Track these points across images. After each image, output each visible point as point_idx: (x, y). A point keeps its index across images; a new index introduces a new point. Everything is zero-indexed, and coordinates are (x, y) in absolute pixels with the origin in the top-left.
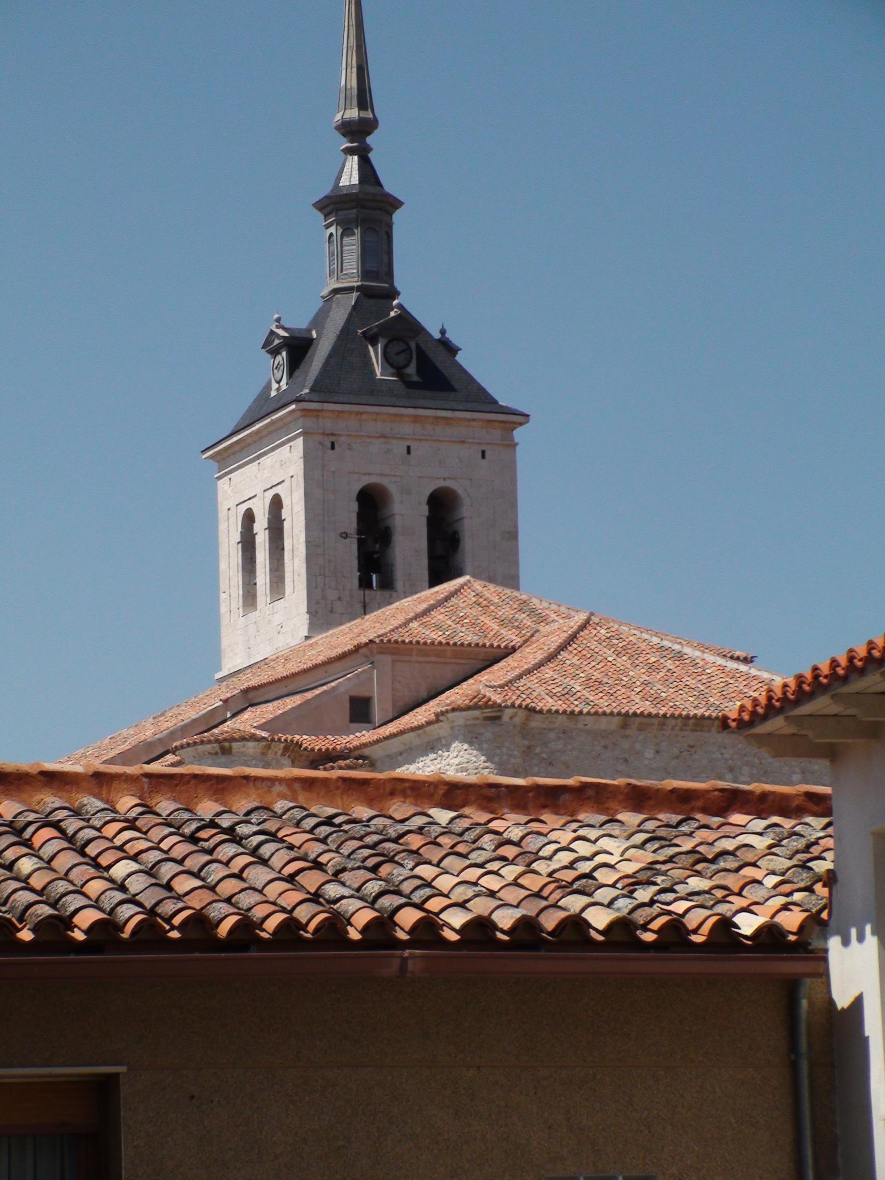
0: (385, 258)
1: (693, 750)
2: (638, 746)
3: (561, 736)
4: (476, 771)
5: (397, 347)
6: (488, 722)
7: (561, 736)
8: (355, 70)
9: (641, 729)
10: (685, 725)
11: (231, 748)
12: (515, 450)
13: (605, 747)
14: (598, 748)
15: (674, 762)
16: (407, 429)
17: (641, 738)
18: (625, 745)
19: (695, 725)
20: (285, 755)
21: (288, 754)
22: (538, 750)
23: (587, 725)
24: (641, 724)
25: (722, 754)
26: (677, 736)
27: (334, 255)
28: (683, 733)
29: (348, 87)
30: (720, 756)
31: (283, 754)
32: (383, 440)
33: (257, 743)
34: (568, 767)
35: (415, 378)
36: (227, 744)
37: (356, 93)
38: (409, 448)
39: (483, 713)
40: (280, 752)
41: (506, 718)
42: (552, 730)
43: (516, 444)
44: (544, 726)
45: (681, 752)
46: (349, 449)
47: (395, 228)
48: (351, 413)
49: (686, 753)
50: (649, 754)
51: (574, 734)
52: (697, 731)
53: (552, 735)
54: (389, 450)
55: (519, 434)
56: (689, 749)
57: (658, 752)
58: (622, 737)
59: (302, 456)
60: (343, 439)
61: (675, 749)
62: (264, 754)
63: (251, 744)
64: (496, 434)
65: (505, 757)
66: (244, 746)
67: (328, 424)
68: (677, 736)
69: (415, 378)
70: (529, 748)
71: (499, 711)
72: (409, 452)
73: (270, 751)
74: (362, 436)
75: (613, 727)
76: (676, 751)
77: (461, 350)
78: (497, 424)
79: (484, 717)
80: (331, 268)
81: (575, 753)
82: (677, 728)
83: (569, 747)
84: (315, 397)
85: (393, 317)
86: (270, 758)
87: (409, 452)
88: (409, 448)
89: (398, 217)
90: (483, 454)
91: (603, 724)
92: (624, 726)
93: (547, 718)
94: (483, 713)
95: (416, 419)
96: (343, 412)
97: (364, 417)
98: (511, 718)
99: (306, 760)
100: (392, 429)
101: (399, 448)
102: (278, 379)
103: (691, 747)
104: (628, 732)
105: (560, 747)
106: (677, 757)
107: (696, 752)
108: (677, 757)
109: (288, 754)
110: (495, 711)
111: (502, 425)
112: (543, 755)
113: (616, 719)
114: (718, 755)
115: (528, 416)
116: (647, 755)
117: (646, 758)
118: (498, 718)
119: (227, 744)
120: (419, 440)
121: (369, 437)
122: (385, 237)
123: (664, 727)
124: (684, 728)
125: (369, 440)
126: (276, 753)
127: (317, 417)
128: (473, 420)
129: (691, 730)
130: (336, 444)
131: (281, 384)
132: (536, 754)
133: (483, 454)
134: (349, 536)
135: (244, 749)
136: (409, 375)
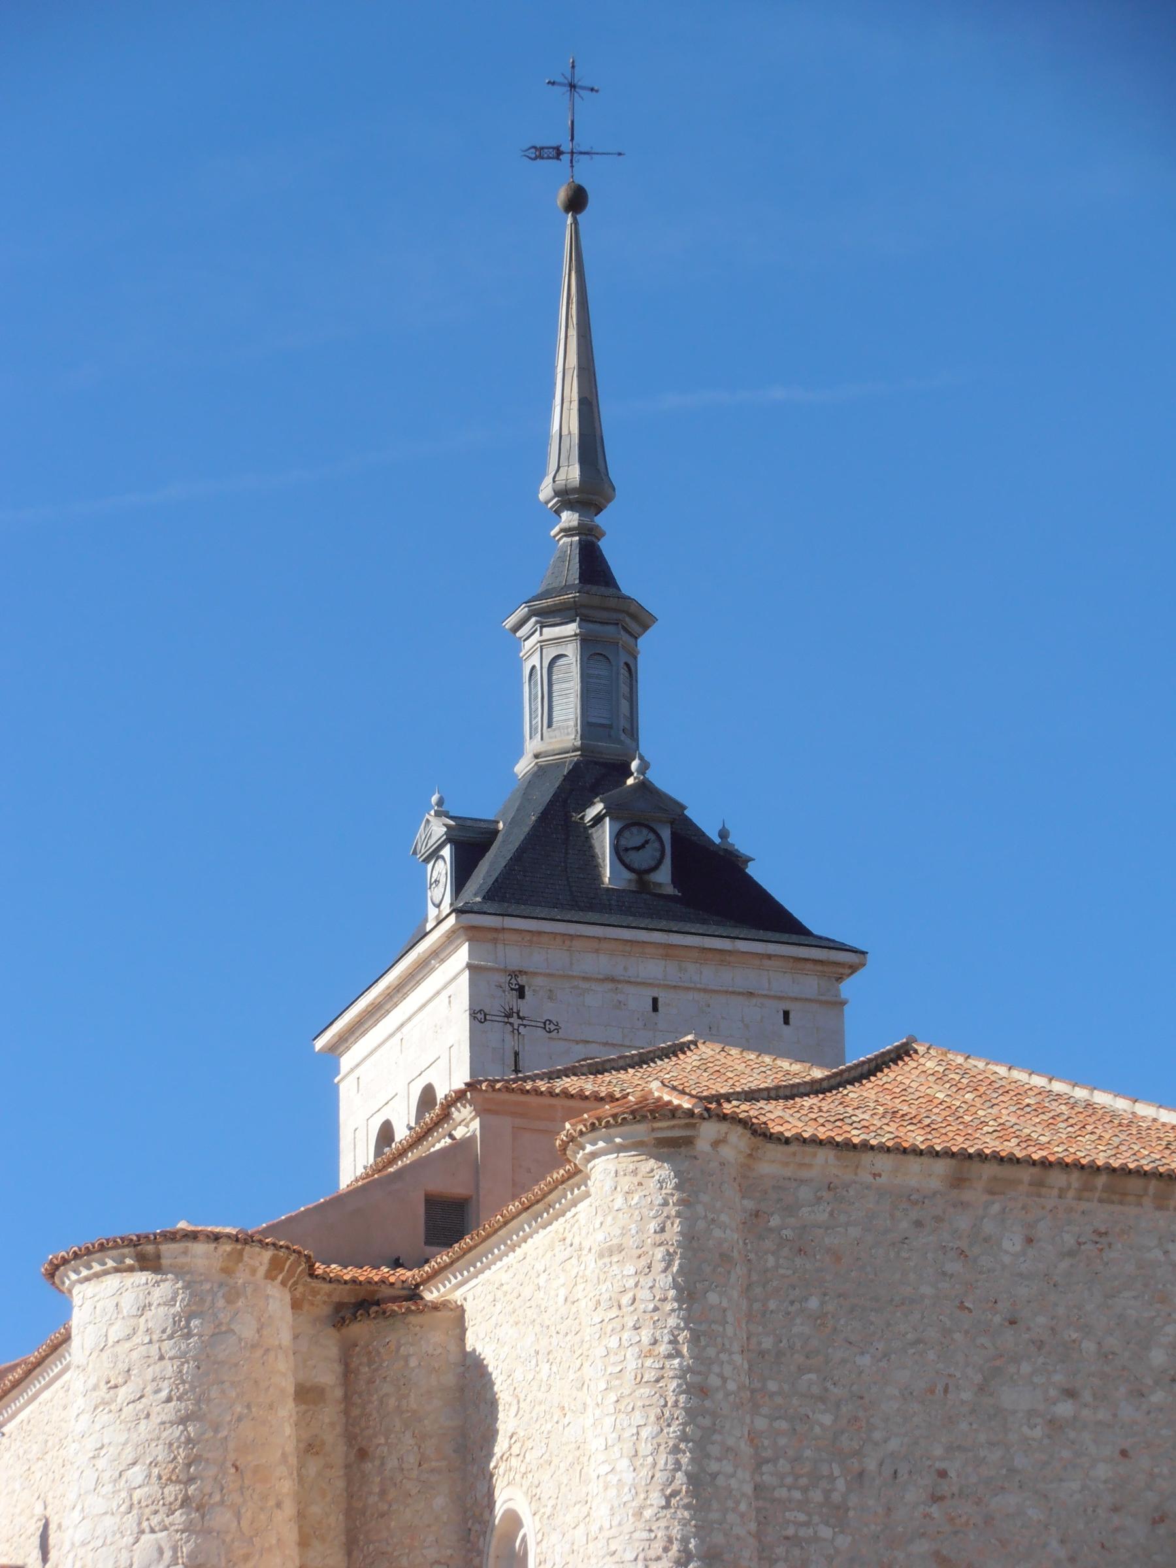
0: (624, 705)
1: (1103, 1240)
2: (988, 1227)
3: (824, 1194)
4: (640, 1251)
5: (635, 837)
6: (665, 1150)
7: (824, 1194)
8: (575, 405)
9: (994, 1189)
10: (1087, 1188)
11: (158, 1256)
12: (842, 1011)
13: (918, 1224)
14: (904, 1225)
15: (1064, 1265)
16: (652, 969)
17: (996, 1208)
18: (963, 1222)
19: (1107, 1188)
20: (273, 1279)
21: (280, 1278)
22: (775, 1221)
23: (880, 1175)
24: (995, 1179)
25: (1166, 1252)
26: (1070, 1210)
27: (537, 716)
28: (1084, 1205)
29: (565, 432)
30: (1162, 1259)
31: (270, 1276)
32: (610, 985)
33: (213, 1246)
34: (838, 1258)
35: (670, 890)
36: (150, 1248)
37: (577, 441)
38: (655, 1001)
39: (653, 1130)
40: (262, 1271)
41: (703, 1145)
42: (802, 1182)
43: (843, 1003)
44: (788, 1172)
45: (1079, 1244)
46: (549, 998)
47: (641, 659)
48: (554, 935)
49: (1089, 1246)
50: (1012, 1243)
51: (852, 1192)
52: (1112, 1202)
53: (805, 1193)
54: (620, 1002)
55: (848, 988)
56: (1096, 1238)
57: (1029, 1241)
58: (954, 1206)
59: (468, 1008)
60: (539, 981)
61: (1066, 1237)
62: (226, 1271)
63: (200, 1248)
64: (810, 985)
65: (701, 1224)
66: (185, 1252)
67: (514, 957)
68: (1070, 1210)
69: (670, 890)
70: (757, 1214)
71: (687, 1126)
72: (655, 1008)
73: (240, 1265)
74: (573, 977)
75: (935, 1184)
76: (1069, 1240)
77: (753, 860)
78: (809, 966)
79: (656, 1139)
80: (534, 723)
81: (854, 1232)
82: (1071, 1194)
83: (843, 1218)
84: (487, 907)
85: (631, 785)
86: (240, 1281)
87: (655, 1008)
88: (655, 1001)
89: (646, 644)
90: (786, 1015)
91: (914, 1173)
92: (958, 1182)
93: (794, 1154)
94: (653, 1130)
95: (669, 951)
96: (539, 933)
97: (577, 944)
98: (716, 1144)
99: (325, 1302)
100: (625, 969)
101: (639, 1000)
102: (437, 902)
103: (1100, 1234)
104: (967, 1195)
105: (823, 1217)
106: (1071, 1254)
107: (1110, 1245)
108: (1071, 1254)
109: (280, 1278)
110: (679, 1127)
111: (819, 968)
112: (784, 1232)
113: (941, 1167)
114: (1157, 1254)
115: (864, 953)
116: (1006, 1244)
117: (1007, 1252)
118: (688, 1142)
119: (150, 1248)
120: (675, 987)
121: (586, 979)
122: (623, 671)
123: (1044, 1191)
124: (1086, 1194)
125: (586, 985)
126: (254, 1272)
127: (495, 941)
128: (769, 957)
129: (1101, 1201)
130: (527, 988)
131: (442, 907)
132: (771, 1230)
133: (786, 1015)
134: (488, 1017)
135: (188, 1259)
136: (660, 885)
